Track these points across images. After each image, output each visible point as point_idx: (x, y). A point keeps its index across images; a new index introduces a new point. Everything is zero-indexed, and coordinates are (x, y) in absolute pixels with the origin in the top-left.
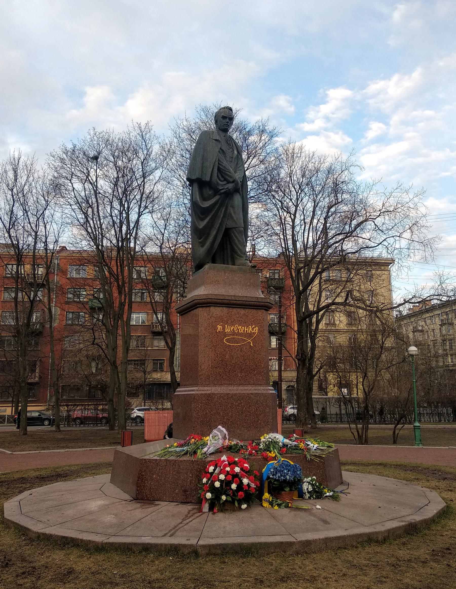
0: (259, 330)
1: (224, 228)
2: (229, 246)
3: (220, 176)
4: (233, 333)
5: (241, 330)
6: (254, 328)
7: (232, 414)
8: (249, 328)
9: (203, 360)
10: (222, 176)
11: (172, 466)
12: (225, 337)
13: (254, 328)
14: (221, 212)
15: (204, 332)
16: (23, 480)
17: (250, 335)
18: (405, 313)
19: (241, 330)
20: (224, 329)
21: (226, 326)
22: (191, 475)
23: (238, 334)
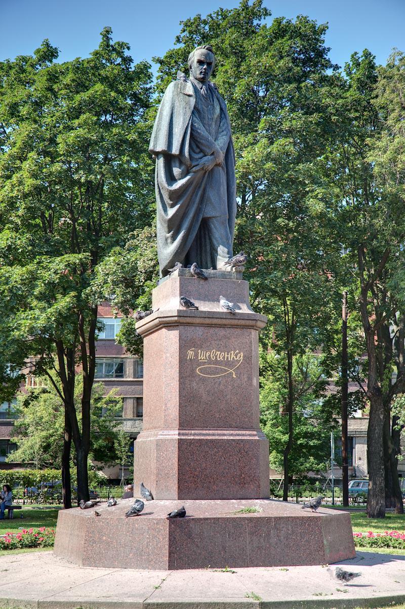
0: (244, 356)
1: (200, 219)
2: (208, 241)
3: (195, 147)
4: (210, 362)
5: (219, 358)
6: (237, 354)
7: (206, 466)
8: (231, 354)
9: (169, 396)
10: (198, 147)
11: (126, 525)
12: (199, 365)
13: (237, 354)
14: (196, 196)
15: (170, 359)
16: (179, 225)
17: (229, 364)
18: (71, 470)
19: (219, 358)
20: (196, 355)
21: (200, 351)
22: (148, 536)
23: (216, 362)
